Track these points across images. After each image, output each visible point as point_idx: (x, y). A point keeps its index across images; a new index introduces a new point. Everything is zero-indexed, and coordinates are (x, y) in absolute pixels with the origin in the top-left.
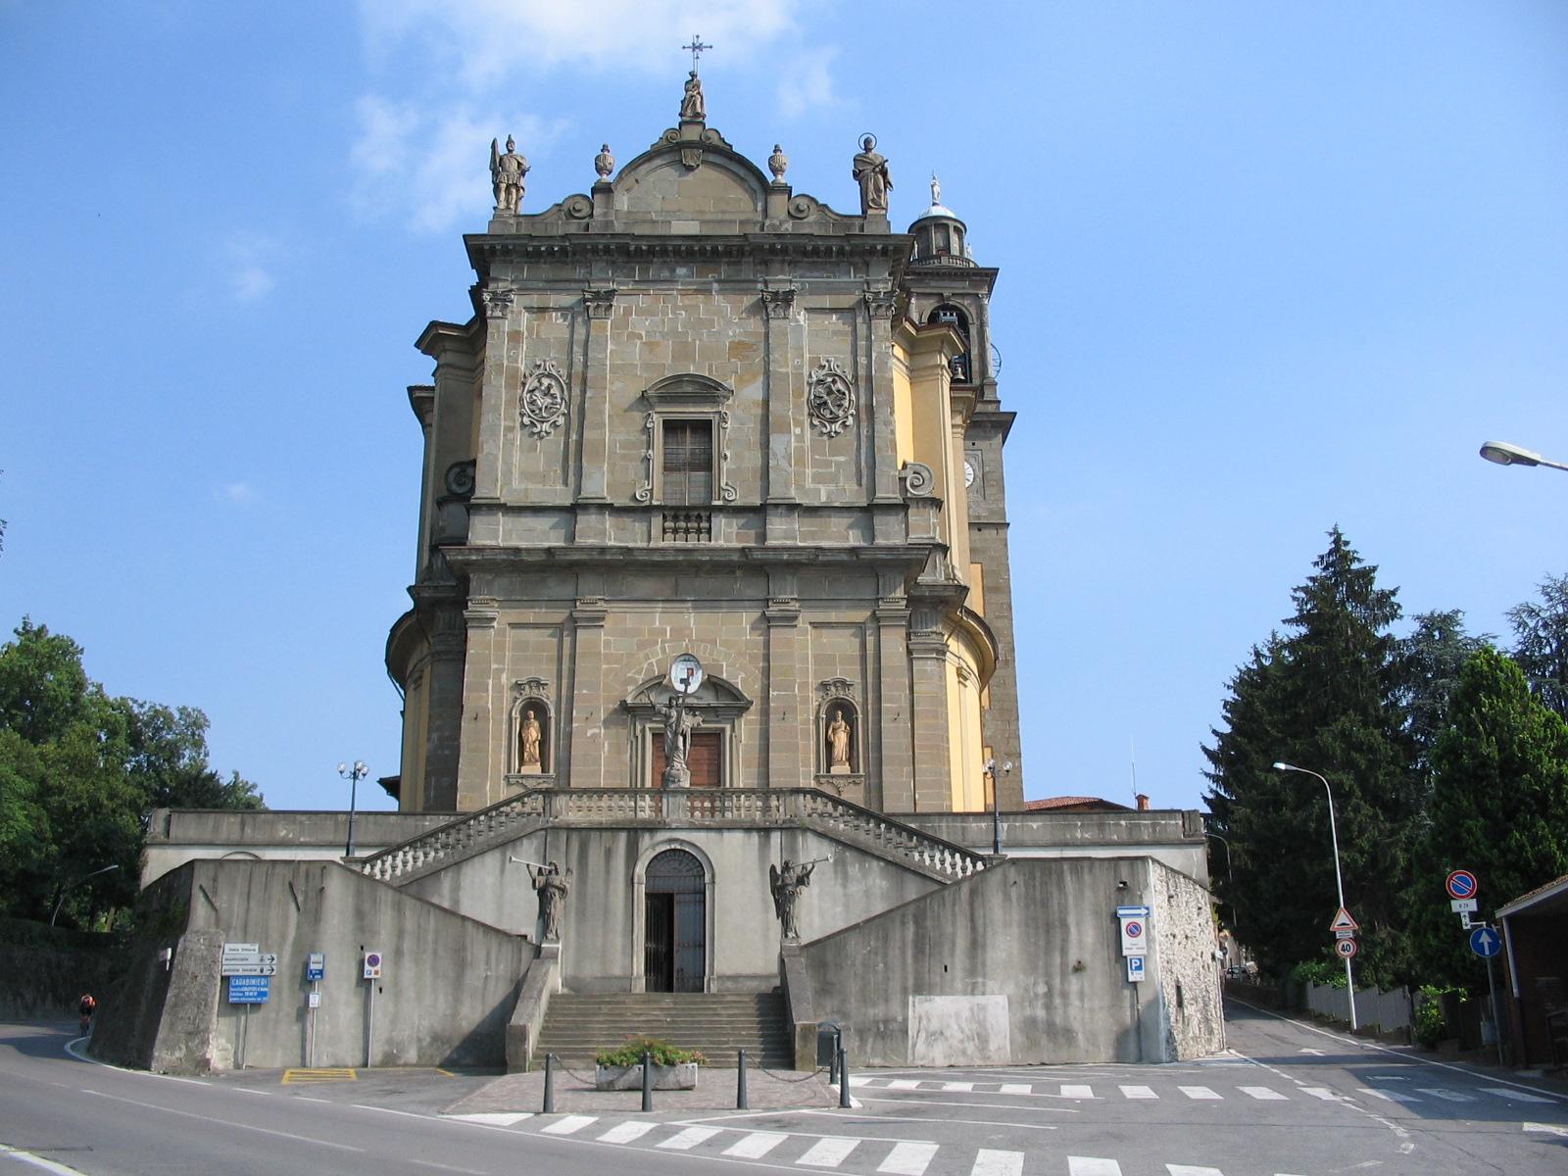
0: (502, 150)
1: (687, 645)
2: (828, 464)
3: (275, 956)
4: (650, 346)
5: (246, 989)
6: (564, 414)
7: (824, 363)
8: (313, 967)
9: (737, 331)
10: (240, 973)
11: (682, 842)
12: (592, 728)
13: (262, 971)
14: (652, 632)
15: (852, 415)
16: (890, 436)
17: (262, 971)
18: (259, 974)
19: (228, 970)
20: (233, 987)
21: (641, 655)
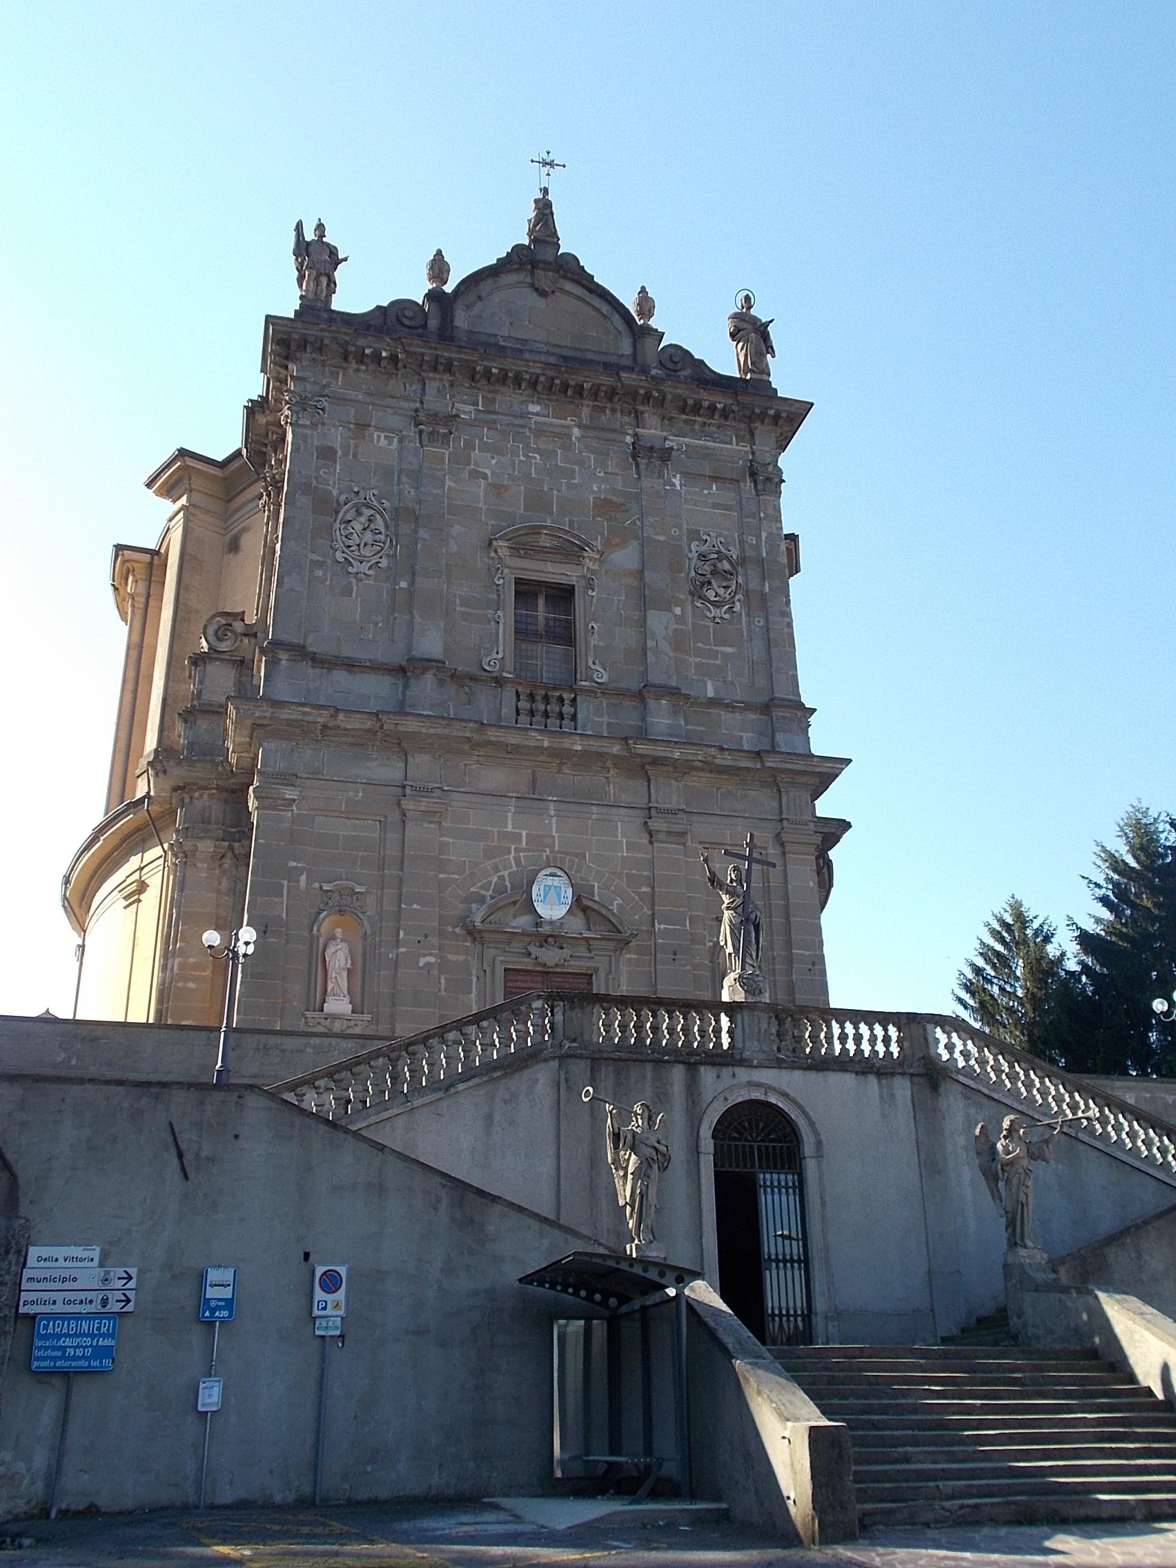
0: (310, 236)
1: (547, 857)
2: (714, 655)
3: (133, 1271)
4: (497, 489)
5: (68, 1342)
6: (388, 555)
7: (705, 537)
8: (211, 1293)
9: (603, 486)
10: (59, 1308)
11: (768, 1088)
12: (425, 955)
13: (105, 1302)
14: (503, 836)
15: (739, 601)
16: (786, 630)
17: (105, 1302)
18: (99, 1309)
19: (32, 1302)
20: (42, 1338)
21: (489, 864)
